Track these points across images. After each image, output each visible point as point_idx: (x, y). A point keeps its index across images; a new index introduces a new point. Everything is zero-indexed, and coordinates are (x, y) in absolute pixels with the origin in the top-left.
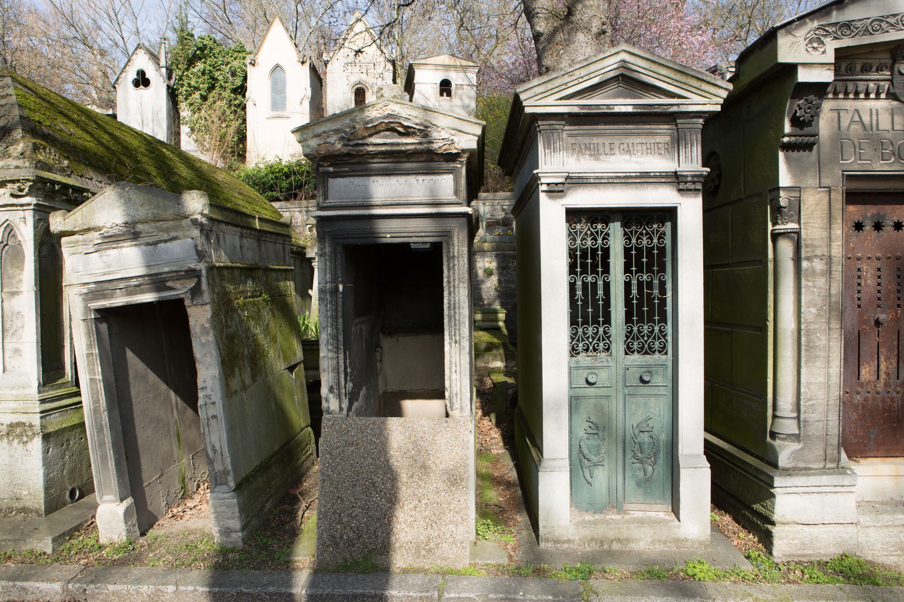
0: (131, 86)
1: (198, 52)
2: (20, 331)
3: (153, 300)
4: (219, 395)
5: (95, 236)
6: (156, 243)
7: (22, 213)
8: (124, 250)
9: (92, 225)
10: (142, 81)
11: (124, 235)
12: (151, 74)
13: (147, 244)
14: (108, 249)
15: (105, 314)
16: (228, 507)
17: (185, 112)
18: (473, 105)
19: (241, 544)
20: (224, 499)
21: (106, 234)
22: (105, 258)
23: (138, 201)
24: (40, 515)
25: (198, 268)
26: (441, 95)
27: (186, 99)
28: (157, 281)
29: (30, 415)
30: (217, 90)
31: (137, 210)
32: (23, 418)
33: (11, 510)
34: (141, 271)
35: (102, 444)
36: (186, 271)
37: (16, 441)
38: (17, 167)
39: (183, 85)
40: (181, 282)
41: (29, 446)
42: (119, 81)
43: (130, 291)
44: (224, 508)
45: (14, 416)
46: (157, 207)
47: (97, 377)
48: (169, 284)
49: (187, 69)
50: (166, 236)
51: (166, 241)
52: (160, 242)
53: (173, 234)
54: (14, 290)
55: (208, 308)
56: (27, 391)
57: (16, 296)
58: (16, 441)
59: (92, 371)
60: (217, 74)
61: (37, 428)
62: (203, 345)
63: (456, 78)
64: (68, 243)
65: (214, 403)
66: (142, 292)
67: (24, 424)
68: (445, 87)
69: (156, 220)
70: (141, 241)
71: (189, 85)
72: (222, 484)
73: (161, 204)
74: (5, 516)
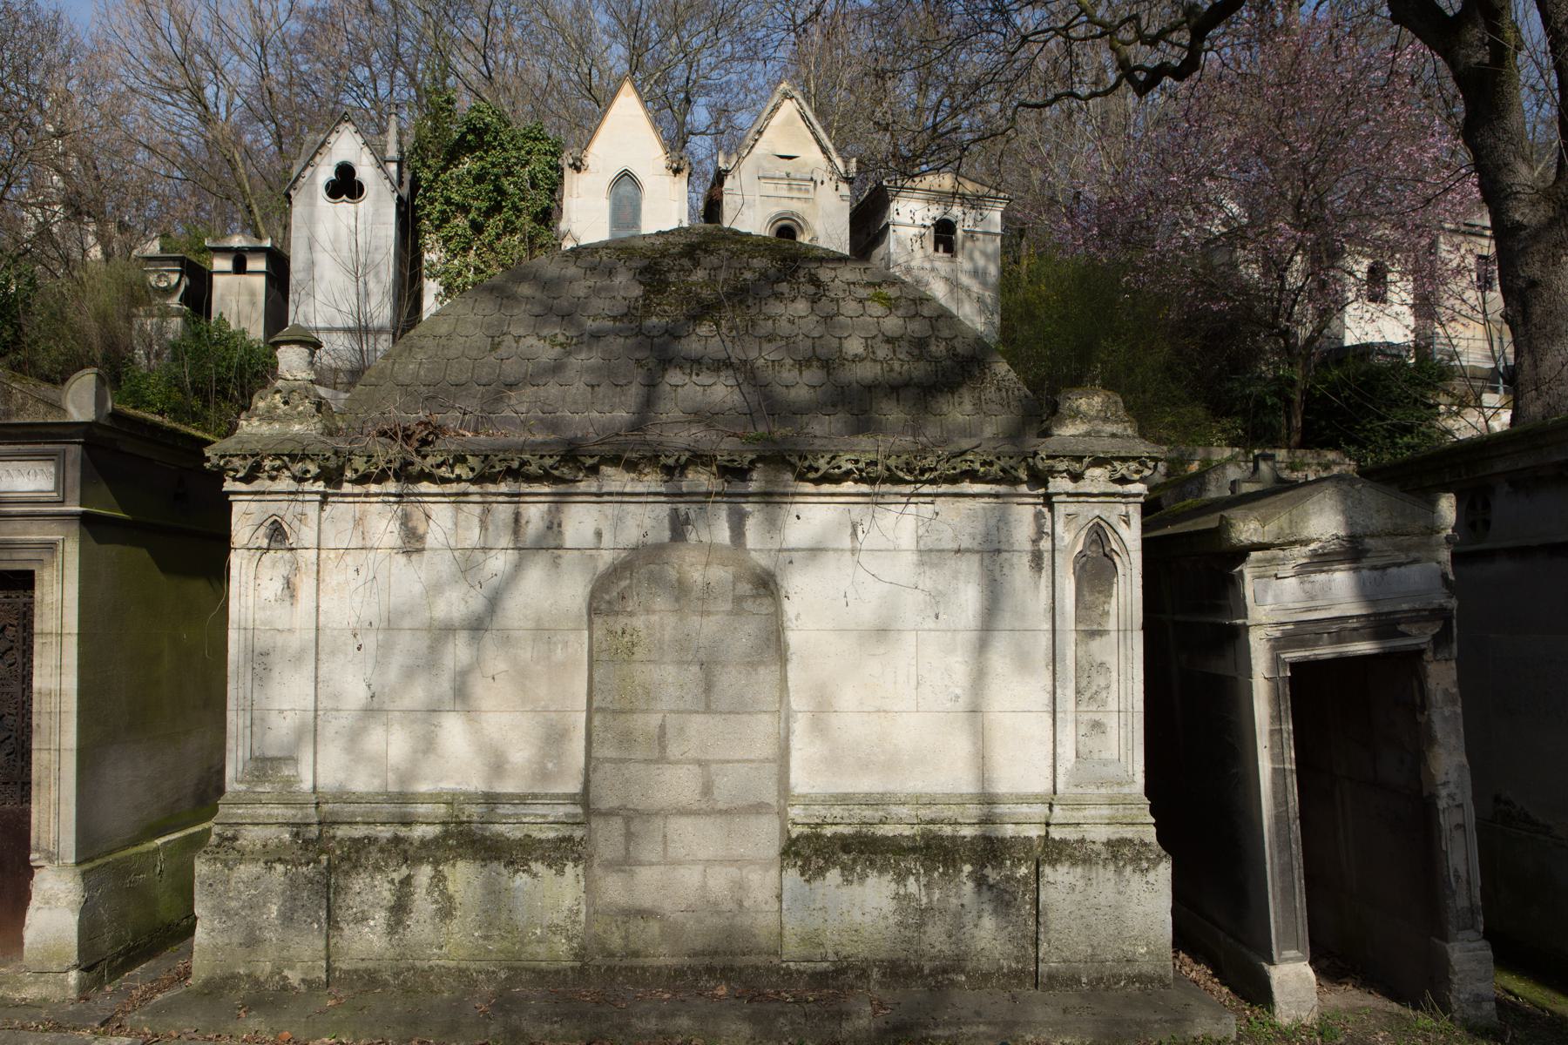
0: (321, 192)
1: (469, 137)
2: (1104, 694)
4: (1469, 793)
5: (1300, 554)
6: (1384, 568)
7: (1123, 507)
10: (345, 185)
12: (366, 171)
13: (1374, 568)
15: (1300, 670)
17: (433, 256)
18: (993, 270)
20: (1474, 950)
22: (1308, 586)
24: (1166, 986)
26: (936, 250)
27: (438, 228)
29: (1140, 828)
30: (507, 213)
32: (1128, 833)
33: (1117, 978)
35: (1286, 870)
36: (1433, 610)
37: (1129, 869)
38: (1113, 435)
39: (432, 201)
41: (1151, 876)
42: (299, 183)
45: (1111, 829)
47: (1287, 766)
48: (1402, 628)
49: (444, 169)
50: (1402, 558)
51: (1400, 565)
52: (1394, 565)
53: (1414, 555)
54: (1095, 627)
55: (1453, 664)
56: (1126, 790)
57: (1098, 639)
58: (1129, 869)
59: (1277, 757)
60: (505, 183)
65: (1460, 806)
67: (1131, 841)
68: (944, 233)
70: (1365, 562)
71: (448, 201)
72: (1465, 928)
74: (1108, 988)
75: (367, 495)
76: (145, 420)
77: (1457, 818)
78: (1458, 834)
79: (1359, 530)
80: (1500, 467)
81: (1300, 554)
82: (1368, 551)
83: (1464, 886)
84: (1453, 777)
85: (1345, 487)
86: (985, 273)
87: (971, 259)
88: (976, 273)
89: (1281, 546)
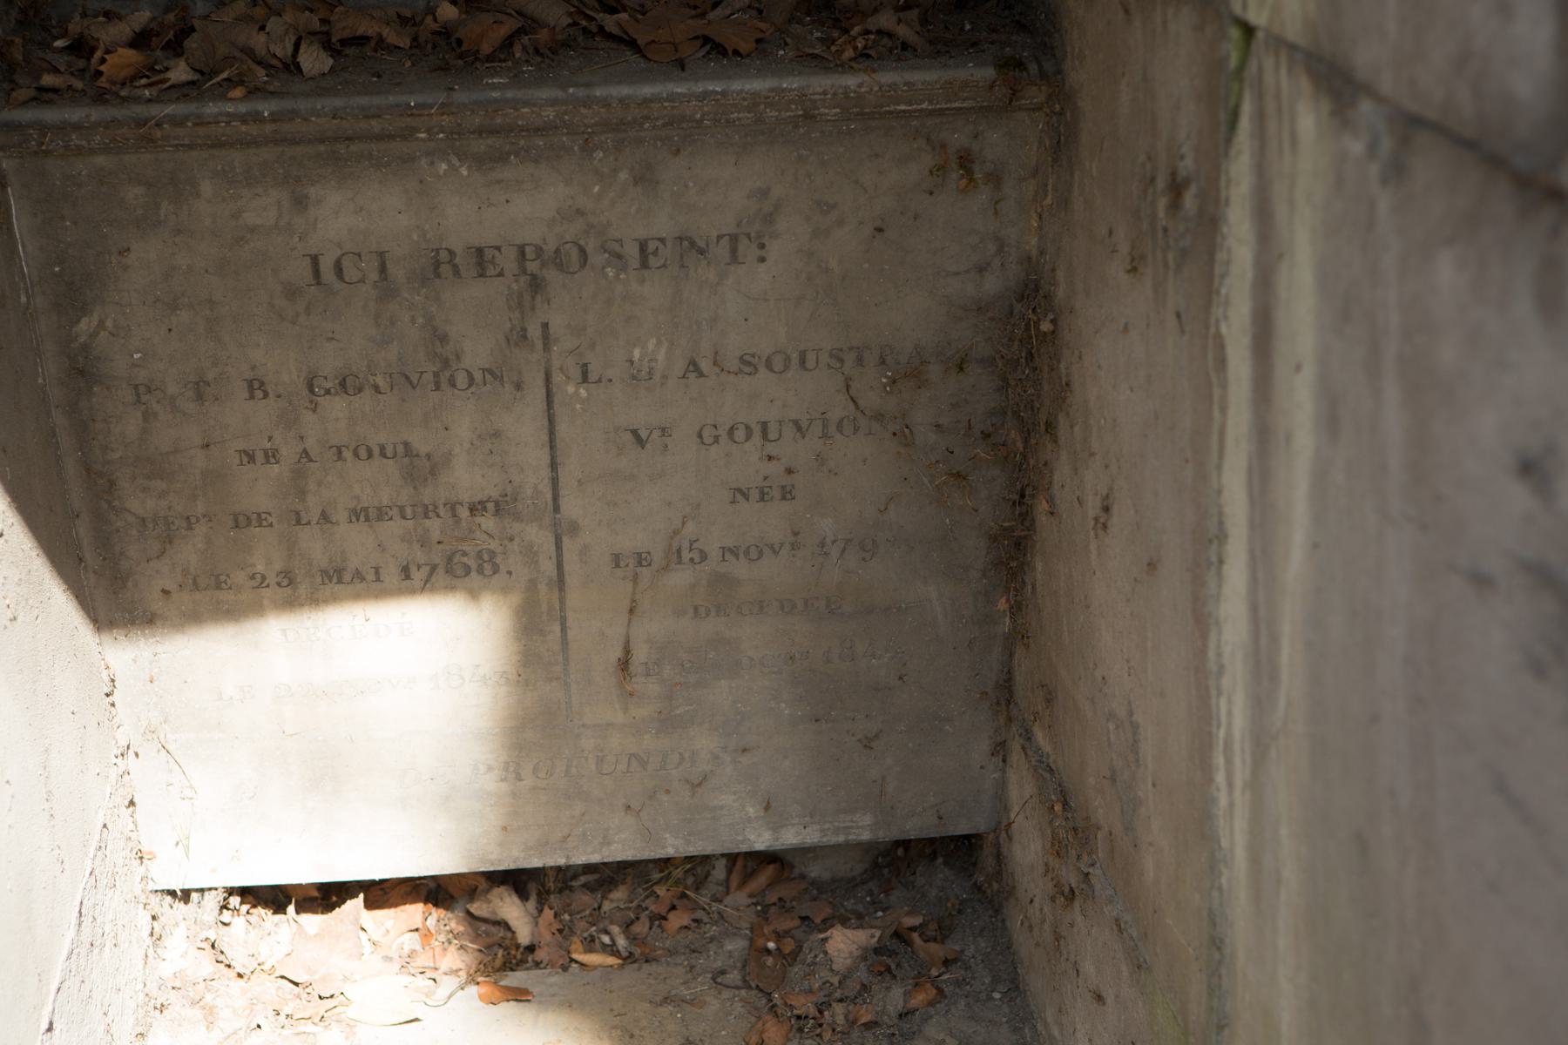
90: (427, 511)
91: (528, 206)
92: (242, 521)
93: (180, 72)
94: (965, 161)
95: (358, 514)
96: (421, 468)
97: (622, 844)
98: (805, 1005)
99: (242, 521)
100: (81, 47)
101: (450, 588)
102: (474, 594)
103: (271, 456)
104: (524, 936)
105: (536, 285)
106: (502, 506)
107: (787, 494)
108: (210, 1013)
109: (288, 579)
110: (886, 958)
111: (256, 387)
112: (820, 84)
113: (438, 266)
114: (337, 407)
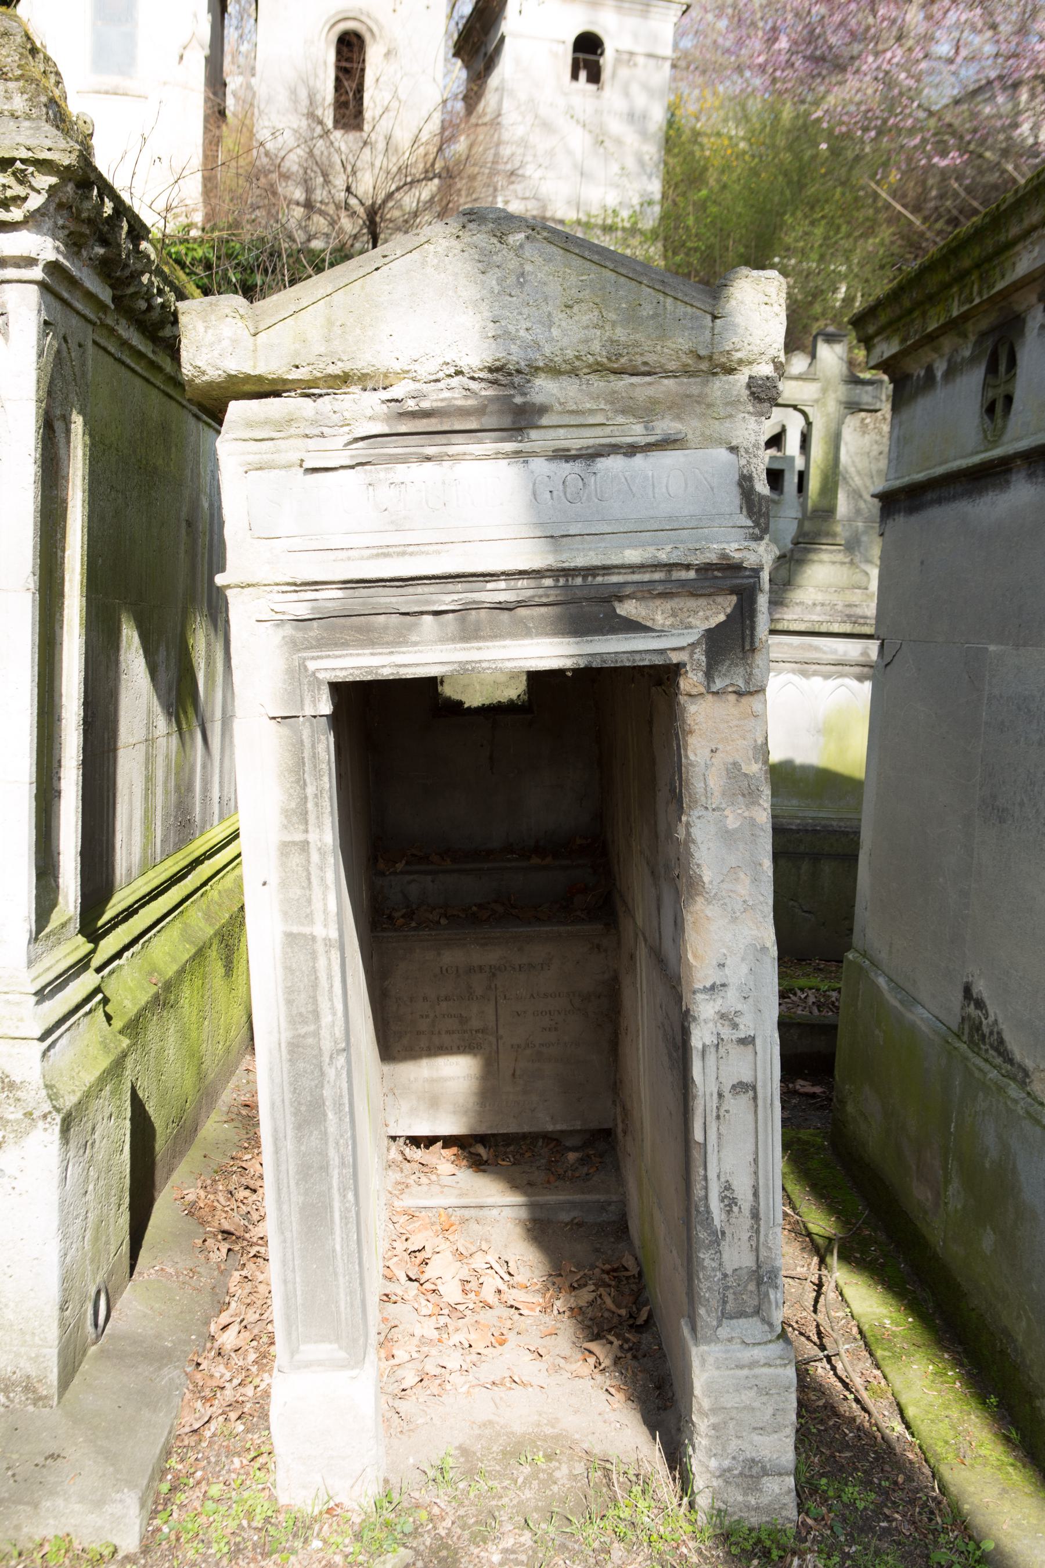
3: (567, 663)
5: (364, 410)
6: (591, 455)
8: (464, 468)
9: (362, 362)
11: (480, 411)
13: (563, 455)
14: (403, 459)
16: (764, 1392)
19: (792, 1512)
20: (753, 1364)
21: (411, 405)
23: (554, 288)
25: (750, 560)
26: (575, 76)
28: (584, 599)
31: (549, 323)
34: (533, 556)
36: (705, 569)
40: (669, 605)
43: (468, 624)
44: (748, 1397)
46: (631, 318)
47: (319, 930)
48: (628, 609)
50: (636, 432)
51: (631, 450)
52: (614, 449)
53: (666, 426)
59: (298, 908)
61: (35, 1097)
62: (728, 836)
63: (617, 34)
64: (250, 425)
65: (747, 1041)
66: (524, 631)
69: (611, 367)
70: (538, 439)
72: (741, 1314)
73: (647, 310)
75: (349, 559)
76: (742, 585)
77: (738, 1067)
78: (738, 1106)
79: (516, 356)
80: (1025, 262)
81: (364, 410)
82: (543, 410)
83: (745, 1222)
84: (737, 973)
85: (481, 238)
86: (644, 117)
87: (626, 94)
88: (632, 117)
89: (308, 389)
90: (465, 1032)
91: (492, 956)
92: (419, 1033)
93: (413, 924)
94: (598, 947)
95: (447, 1032)
96: (463, 1020)
97: (510, 1127)
98: (561, 1171)
99: (419, 1033)
100: (390, 917)
101: (469, 1053)
102: (475, 1055)
103: (427, 1016)
104: (485, 1157)
105: (494, 975)
106: (484, 1031)
107: (556, 1029)
108: (402, 1171)
109: (429, 1049)
110: (583, 1161)
111: (425, 999)
112: (562, 928)
113: (470, 970)
114: (444, 1004)
